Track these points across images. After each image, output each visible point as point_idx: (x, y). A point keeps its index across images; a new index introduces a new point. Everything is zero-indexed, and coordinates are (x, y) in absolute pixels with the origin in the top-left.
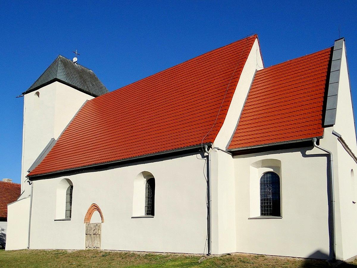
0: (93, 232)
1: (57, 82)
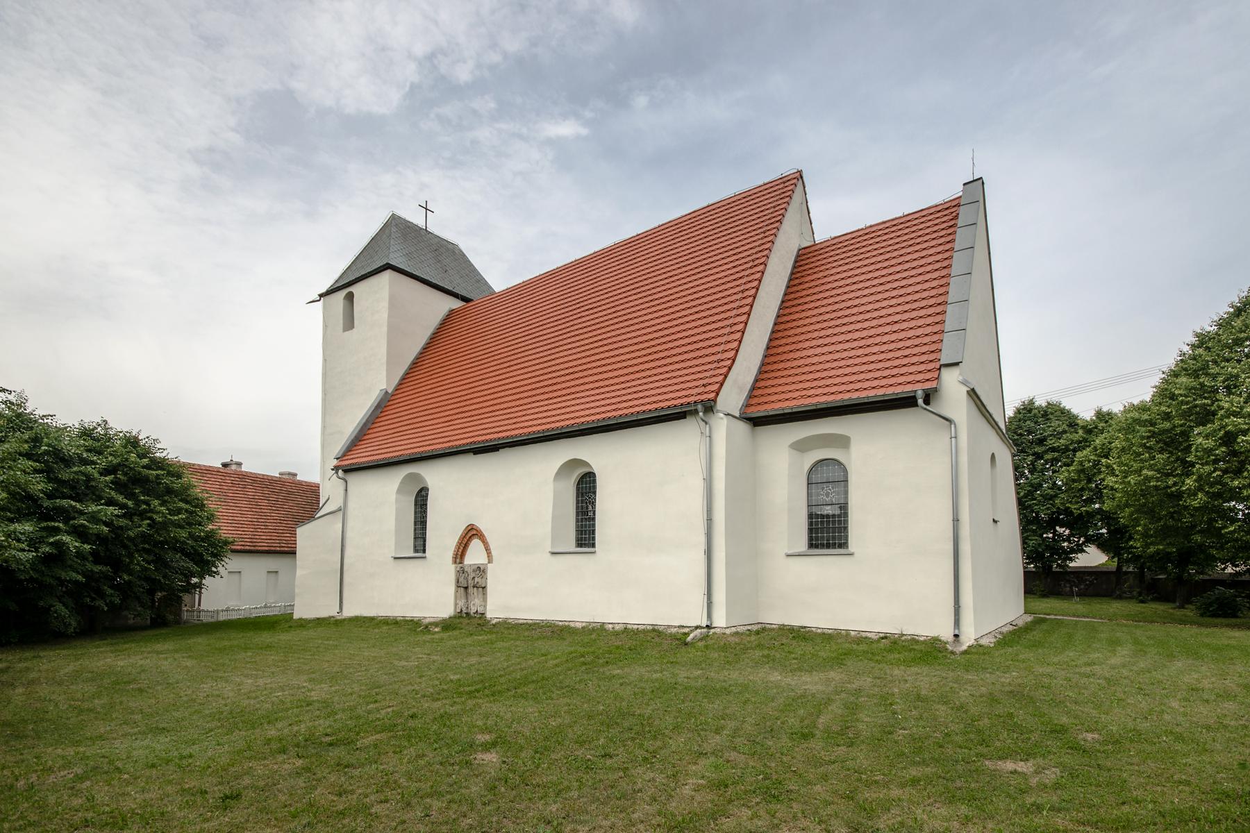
0: (471, 583)
1: (388, 274)
